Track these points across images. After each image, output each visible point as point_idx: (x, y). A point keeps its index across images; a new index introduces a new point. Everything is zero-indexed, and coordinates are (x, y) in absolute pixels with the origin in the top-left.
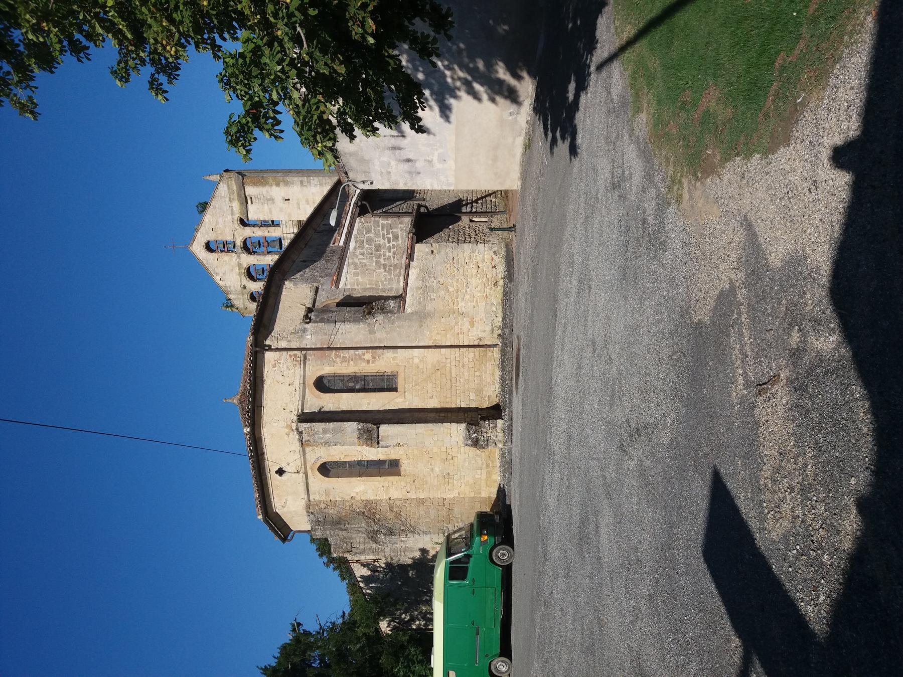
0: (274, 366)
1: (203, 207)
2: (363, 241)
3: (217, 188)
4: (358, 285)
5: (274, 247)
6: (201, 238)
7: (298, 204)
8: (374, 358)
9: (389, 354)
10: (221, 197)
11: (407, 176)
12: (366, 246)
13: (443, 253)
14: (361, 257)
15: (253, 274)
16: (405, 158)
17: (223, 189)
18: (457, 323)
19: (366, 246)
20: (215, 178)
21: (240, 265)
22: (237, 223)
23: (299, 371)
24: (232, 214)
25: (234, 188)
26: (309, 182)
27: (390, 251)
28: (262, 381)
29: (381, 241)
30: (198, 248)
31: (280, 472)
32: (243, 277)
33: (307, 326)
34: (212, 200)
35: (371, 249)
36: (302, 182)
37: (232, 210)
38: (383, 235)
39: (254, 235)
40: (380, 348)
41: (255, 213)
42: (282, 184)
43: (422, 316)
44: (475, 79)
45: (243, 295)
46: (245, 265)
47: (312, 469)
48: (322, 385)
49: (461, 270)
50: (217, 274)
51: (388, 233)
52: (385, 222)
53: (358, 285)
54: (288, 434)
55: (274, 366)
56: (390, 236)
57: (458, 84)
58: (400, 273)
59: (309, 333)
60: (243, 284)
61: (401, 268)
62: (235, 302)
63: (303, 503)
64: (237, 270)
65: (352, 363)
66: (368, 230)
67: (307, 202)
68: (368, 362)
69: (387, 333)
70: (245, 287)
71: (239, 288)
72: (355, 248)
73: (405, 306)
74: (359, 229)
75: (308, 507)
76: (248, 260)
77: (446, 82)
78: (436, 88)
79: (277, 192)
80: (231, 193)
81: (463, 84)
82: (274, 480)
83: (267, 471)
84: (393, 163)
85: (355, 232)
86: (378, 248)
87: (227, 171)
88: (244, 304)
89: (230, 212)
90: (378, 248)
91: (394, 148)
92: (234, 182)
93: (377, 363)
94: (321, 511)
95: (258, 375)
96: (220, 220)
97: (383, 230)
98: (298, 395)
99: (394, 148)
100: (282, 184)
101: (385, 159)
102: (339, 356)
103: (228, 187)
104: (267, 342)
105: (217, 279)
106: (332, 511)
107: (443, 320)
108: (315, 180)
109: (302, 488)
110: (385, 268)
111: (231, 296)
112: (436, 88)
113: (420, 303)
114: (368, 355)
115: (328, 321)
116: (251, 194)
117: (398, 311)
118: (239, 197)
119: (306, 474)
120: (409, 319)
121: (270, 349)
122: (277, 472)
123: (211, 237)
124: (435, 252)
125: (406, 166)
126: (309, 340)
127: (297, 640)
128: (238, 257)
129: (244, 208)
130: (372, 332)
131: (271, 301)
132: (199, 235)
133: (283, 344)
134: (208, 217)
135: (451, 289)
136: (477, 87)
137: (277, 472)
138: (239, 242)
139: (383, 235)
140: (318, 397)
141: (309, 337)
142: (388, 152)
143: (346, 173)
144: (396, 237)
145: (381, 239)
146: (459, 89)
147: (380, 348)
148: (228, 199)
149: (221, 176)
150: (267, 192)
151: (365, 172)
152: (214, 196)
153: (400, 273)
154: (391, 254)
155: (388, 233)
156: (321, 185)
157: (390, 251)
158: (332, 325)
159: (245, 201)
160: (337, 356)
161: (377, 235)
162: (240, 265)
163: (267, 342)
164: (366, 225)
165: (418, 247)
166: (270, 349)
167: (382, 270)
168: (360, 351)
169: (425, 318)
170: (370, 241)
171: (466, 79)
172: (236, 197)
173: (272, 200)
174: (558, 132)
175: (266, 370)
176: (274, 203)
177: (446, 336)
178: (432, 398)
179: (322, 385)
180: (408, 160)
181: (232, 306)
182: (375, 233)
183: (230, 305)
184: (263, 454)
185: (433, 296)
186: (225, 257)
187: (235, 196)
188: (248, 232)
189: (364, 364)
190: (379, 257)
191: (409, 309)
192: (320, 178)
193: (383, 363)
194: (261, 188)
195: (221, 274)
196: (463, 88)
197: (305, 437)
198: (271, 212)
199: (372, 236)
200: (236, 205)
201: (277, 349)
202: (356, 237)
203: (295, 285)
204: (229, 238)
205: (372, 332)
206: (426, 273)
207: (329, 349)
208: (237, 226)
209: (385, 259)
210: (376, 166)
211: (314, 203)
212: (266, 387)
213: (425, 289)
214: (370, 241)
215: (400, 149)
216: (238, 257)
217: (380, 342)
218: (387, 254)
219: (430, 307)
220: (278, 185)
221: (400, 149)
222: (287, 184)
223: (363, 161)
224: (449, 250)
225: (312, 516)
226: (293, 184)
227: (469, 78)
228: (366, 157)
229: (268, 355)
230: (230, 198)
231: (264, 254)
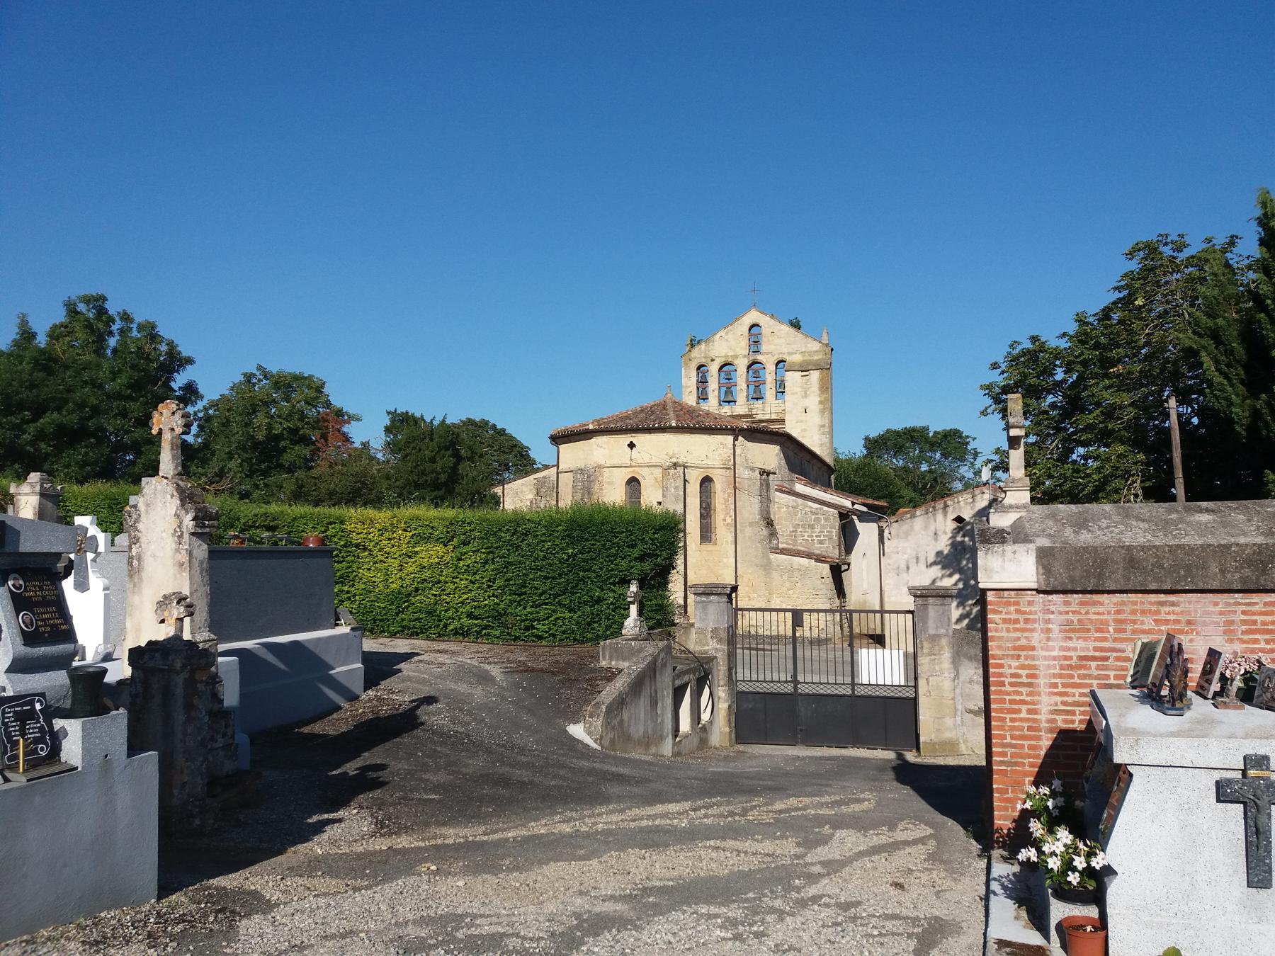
0: (721, 443)
1: (796, 325)
2: (817, 514)
3: (815, 340)
4: (778, 508)
5: (755, 392)
6: (764, 320)
7: (802, 421)
8: (728, 525)
9: (731, 537)
10: (806, 343)
11: (895, 567)
12: (813, 517)
13: (822, 586)
14: (804, 512)
15: (725, 369)
16: (910, 566)
17: (815, 346)
18: (759, 596)
19: (813, 517)
20: (825, 340)
21: (736, 357)
22: (780, 357)
23: (718, 463)
24: (789, 353)
25: (816, 358)
26: (824, 433)
27: (808, 536)
28: (710, 434)
29: (818, 529)
30: (753, 316)
31: (632, 445)
32: (724, 359)
33: (757, 473)
34: (803, 334)
35: (811, 520)
36: (823, 426)
37: (793, 353)
38: (823, 532)
39: (767, 374)
40: (736, 530)
41: (793, 379)
42: (822, 407)
43: (767, 567)
44: (971, 620)
45: (705, 358)
46: (736, 362)
47: (633, 471)
48: (706, 481)
49: (807, 601)
50: (727, 333)
51: (824, 536)
52: (834, 534)
53: (778, 508)
54: (667, 454)
55: (721, 443)
56: (822, 538)
57: (968, 608)
58: (789, 544)
59: (751, 473)
60: (717, 359)
61: (794, 546)
62: (696, 349)
63: (602, 462)
64: (730, 354)
65: (724, 506)
66: (826, 520)
67: (804, 431)
68: (725, 520)
69: (750, 537)
70: (713, 360)
71: (712, 354)
72: (811, 507)
73: (777, 553)
74: (828, 512)
75: (600, 467)
76: (742, 365)
77: (968, 600)
78: (964, 592)
79: (814, 401)
80: (810, 353)
81: (968, 612)
82: (625, 439)
83: (634, 435)
84: (906, 556)
85: (825, 508)
86: (812, 527)
87: (832, 350)
88: (695, 358)
89: (791, 351)
90: (812, 527)
91: (917, 558)
92: (820, 357)
93: (724, 528)
94: (596, 478)
95: (715, 432)
96: (782, 341)
97: (827, 532)
98: (699, 463)
99: (917, 558)
100: (822, 407)
101: (909, 551)
102: (729, 496)
103: (816, 351)
104: (740, 438)
105: (722, 333)
106: (596, 487)
107: (763, 584)
108: (825, 439)
109: (616, 462)
110: (793, 531)
111: (703, 346)
112: (964, 592)
113: (779, 566)
114: (730, 520)
115: (761, 490)
116: (812, 376)
117: (771, 548)
118: (808, 363)
119: (631, 466)
120: (763, 557)
121: (736, 439)
122: (631, 442)
123: (765, 330)
124: (823, 580)
125: (903, 566)
126: (743, 473)
127: (393, 421)
128: (745, 356)
129: (796, 368)
130: (751, 524)
131: (768, 437)
132: (768, 318)
133: (738, 451)
134: (786, 329)
135: (791, 592)
136: (966, 621)
137: (631, 442)
138: (759, 358)
139: (823, 532)
140: (697, 478)
141: (747, 473)
142: (915, 553)
143: (897, 521)
144: (821, 542)
145: (819, 530)
146: (963, 609)
147: (736, 530)
148: (803, 350)
149: (827, 345)
150: (814, 392)
151: (898, 535)
152: (807, 336)
153: (789, 544)
154: (806, 538)
155: (824, 536)
156: (821, 445)
157: (808, 536)
158: (758, 493)
159: (804, 369)
160: (729, 494)
161: (823, 526)
162: (736, 357)
163: (740, 438)
164: (832, 518)
165: (827, 566)
166: (736, 439)
167: (791, 530)
168: (732, 513)
169: (765, 570)
170: (817, 520)
171: (971, 614)
172: (805, 358)
173: (806, 396)
174: (334, 773)
175: (718, 437)
176: (802, 397)
177: (747, 586)
178: (695, 574)
179: (706, 481)
180: (908, 568)
181: (692, 346)
182: (824, 525)
183: (693, 344)
184: (650, 433)
185: (785, 577)
186: (744, 343)
187: (807, 358)
188: (771, 367)
189: (722, 517)
190: (803, 527)
191: (773, 556)
192: (828, 445)
193: (723, 532)
194: (818, 386)
195: (726, 337)
196: (965, 612)
197: (672, 472)
198: (793, 394)
199: (822, 523)
200: (797, 358)
201: (734, 445)
202: (821, 509)
203: (777, 455)
204: (764, 348)
205: (751, 524)
206: (805, 572)
207: (735, 488)
208: (777, 357)
209: (801, 532)
210: (902, 544)
211: (803, 437)
212: (706, 437)
213: (791, 571)
214: (817, 520)
215: (917, 563)
216: (745, 356)
217: (741, 531)
218: (806, 534)
219: (775, 574)
220: (821, 402)
221: (917, 563)
222: (822, 411)
223: (907, 534)
224: (824, 591)
225: (593, 470)
226: (822, 417)
227: (972, 616)
228: (910, 537)
229: (731, 438)
230: (805, 352)
231: (747, 381)
